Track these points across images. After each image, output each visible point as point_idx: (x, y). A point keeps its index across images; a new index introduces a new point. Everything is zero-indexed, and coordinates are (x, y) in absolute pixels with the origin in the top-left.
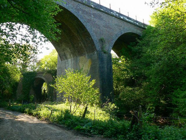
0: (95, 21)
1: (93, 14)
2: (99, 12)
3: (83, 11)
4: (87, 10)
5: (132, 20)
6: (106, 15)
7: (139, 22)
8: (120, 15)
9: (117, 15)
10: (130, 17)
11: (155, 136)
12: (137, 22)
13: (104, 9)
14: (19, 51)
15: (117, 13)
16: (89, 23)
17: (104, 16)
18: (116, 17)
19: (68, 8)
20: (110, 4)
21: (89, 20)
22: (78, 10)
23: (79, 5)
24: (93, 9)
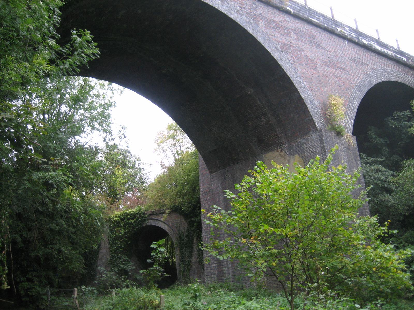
0: (302, 50)
1: (294, 30)
2: (307, 26)
3: (270, 22)
4: (276, 19)
5: (390, 50)
6: (328, 35)
7: (409, 55)
8: (361, 36)
9: (353, 34)
10: (383, 40)
12: (402, 53)
13: (318, 19)
14: (359, 254)
15: (351, 29)
16: (286, 52)
17: (322, 36)
18: (351, 41)
20: (331, 9)
22: (255, 18)
24: (292, 18)
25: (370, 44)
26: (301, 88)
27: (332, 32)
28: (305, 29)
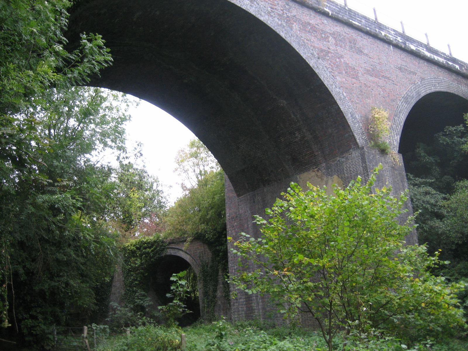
0: (342, 57)
1: (333, 34)
2: (347, 30)
3: (305, 25)
4: (312, 22)
5: (441, 57)
6: (371, 40)
7: (462, 62)
8: (408, 41)
9: (399, 39)
10: (432, 45)
11: (74, 237)
12: (454, 61)
13: (360, 22)
15: (397, 33)
16: (323, 59)
17: (364, 41)
18: (396, 46)
19: (257, 13)
20: (374, 10)
21: (322, 51)
22: (288, 20)
23: (288, 5)
24: (330, 21)
25: (419, 50)
26: (340, 99)
27: (375, 37)
28: (345, 33)
